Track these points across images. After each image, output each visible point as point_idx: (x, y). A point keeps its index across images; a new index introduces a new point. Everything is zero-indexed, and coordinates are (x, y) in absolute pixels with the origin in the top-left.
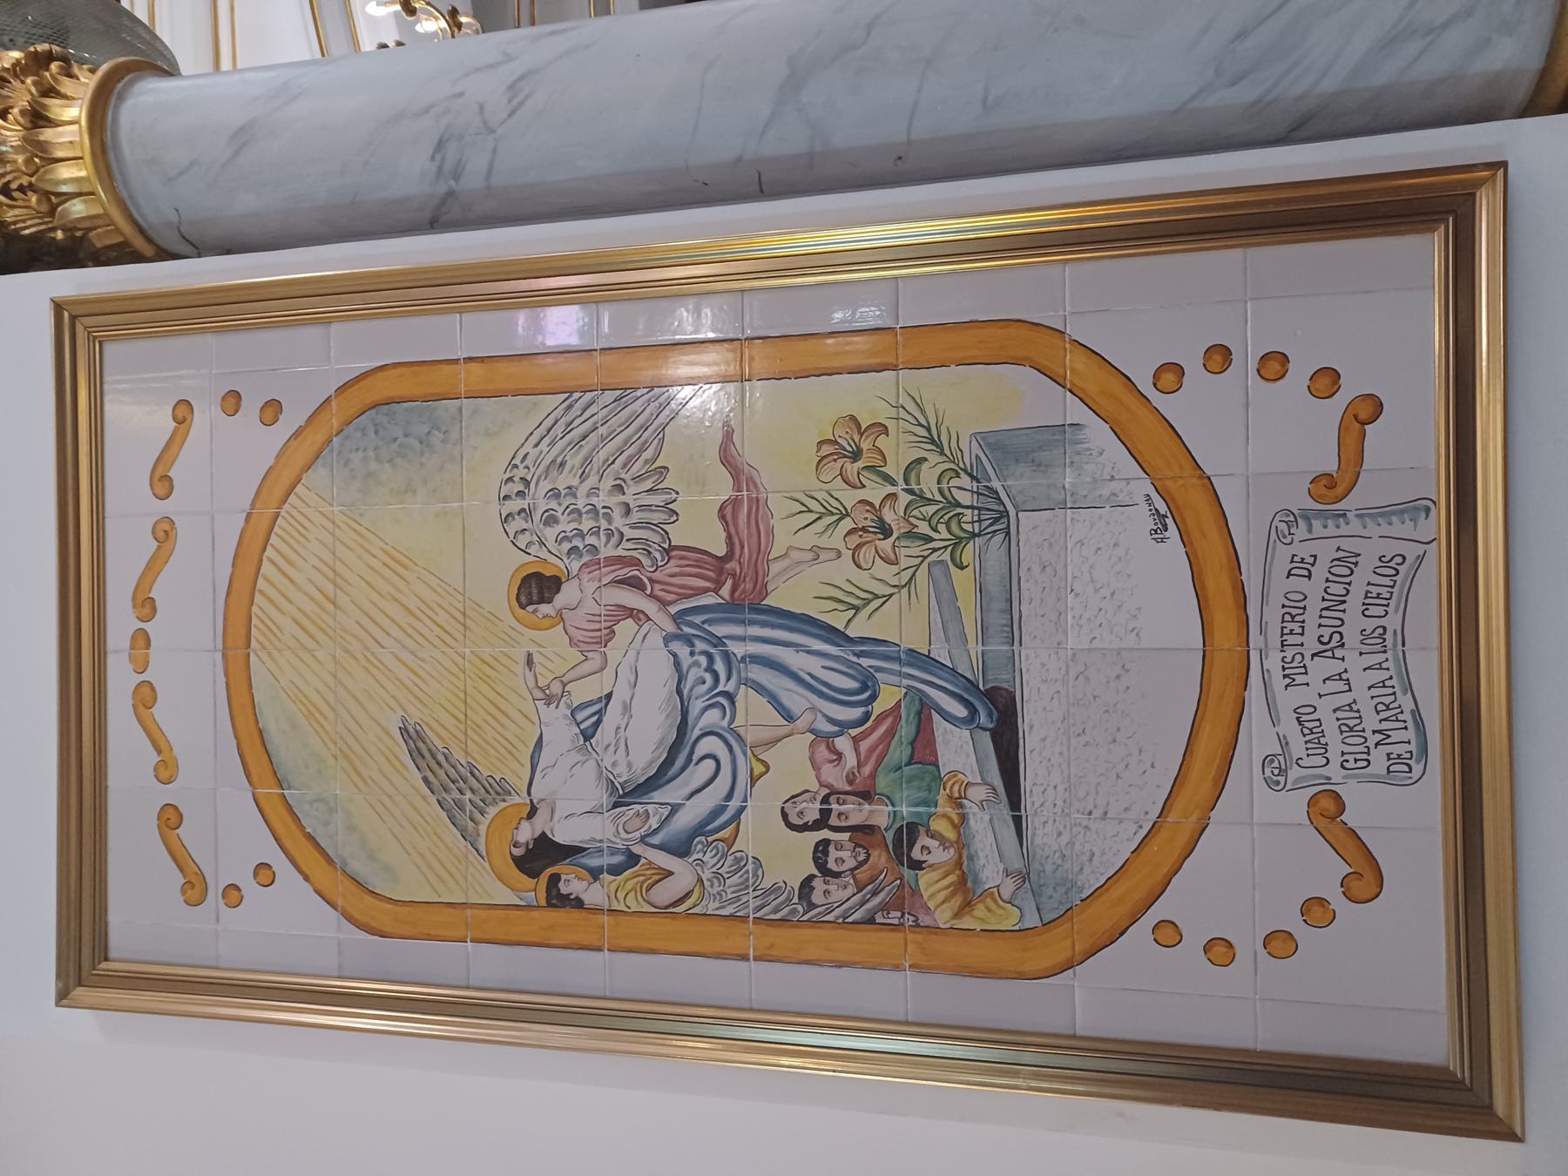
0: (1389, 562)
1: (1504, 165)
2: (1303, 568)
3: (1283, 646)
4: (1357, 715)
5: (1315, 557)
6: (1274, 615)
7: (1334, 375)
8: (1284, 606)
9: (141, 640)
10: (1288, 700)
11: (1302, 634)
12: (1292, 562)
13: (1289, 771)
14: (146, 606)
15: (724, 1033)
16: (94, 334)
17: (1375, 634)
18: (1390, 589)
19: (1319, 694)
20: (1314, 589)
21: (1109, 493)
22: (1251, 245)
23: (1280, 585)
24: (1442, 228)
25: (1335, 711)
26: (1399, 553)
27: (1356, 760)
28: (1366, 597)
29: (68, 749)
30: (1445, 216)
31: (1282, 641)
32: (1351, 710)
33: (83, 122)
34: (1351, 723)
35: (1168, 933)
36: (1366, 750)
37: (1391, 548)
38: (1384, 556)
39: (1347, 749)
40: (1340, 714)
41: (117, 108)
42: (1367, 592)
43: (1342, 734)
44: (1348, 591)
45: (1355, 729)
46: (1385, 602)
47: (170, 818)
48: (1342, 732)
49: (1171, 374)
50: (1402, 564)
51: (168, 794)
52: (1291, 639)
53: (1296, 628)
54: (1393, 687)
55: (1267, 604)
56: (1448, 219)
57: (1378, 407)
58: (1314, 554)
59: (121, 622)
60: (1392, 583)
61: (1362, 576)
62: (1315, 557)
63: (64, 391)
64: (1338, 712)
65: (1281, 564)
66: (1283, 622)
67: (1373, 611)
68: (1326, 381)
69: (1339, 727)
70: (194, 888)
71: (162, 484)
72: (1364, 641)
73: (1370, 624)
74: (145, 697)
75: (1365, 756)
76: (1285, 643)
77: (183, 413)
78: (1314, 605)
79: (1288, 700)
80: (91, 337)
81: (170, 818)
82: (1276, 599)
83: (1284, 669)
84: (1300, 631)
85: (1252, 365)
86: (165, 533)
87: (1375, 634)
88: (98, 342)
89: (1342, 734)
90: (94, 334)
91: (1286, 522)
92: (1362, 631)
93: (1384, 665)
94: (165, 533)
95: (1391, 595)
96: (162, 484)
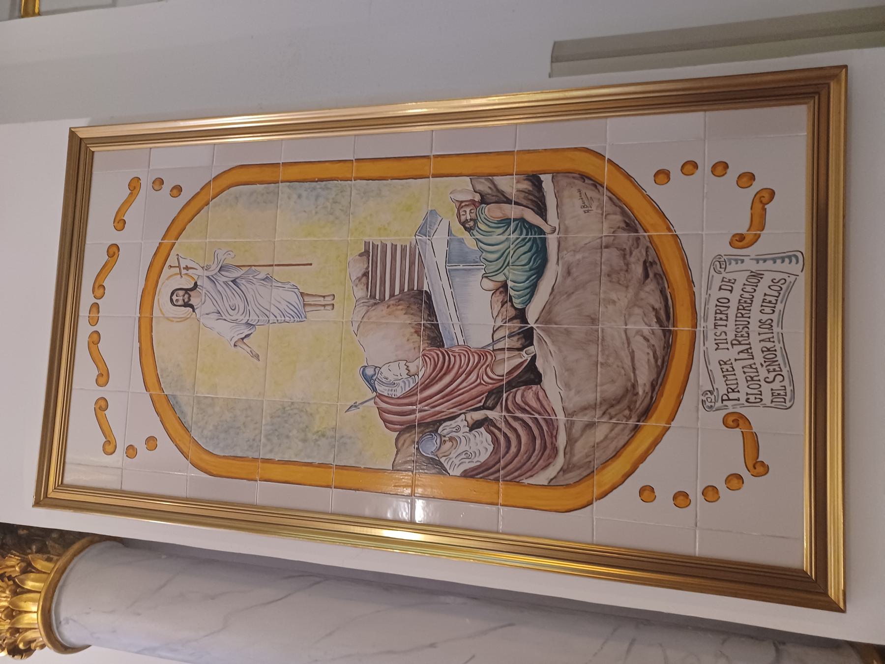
0: (777, 283)
1: (846, 67)
2: (728, 285)
3: (715, 326)
4: (755, 371)
5: (735, 280)
6: (712, 309)
7: (752, 177)
8: (717, 306)
9: (95, 307)
10: (715, 357)
11: (727, 320)
12: (723, 281)
13: (716, 403)
14: (99, 288)
15: (401, 112)
16: (56, 486)
17: (767, 323)
18: (776, 298)
19: (731, 293)
20: (734, 298)
21: (626, 299)
22: (709, 110)
23: (716, 294)
24: (812, 102)
25: (743, 368)
26: (783, 278)
27: (756, 398)
28: (763, 302)
29: (60, 300)
30: (814, 95)
31: (715, 323)
32: (751, 368)
33: (43, 594)
34: (752, 375)
35: (647, 493)
36: (760, 393)
37: (778, 276)
38: (775, 279)
39: (750, 391)
40: (746, 370)
41: (60, 633)
42: (764, 299)
43: (747, 383)
44: (755, 290)
45: (771, 349)
46: (773, 305)
47: (102, 406)
48: (747, 381)
49: (662, 176)
50: (784, 284)
51: (101, 392)
52: (720, 323)
53: (724, 317)
54: (774, 342)
55: (709, 364)
56: (815, 97)
57: (772, 194)
58: (740, 399)
59: (87, 298)
60: (777, 295)
61: (763, 287)
62: (735, 280)
63: (51, 396)
64: (745, 368)
65: (717, 282)
66: (716, 313)
67: (768, 310)
68: (747, 178)
69: (746, 378)
70: (109, 447)
71: (120, 223)
72: (761, 327)
73: (765, 317)
74: (95, 339)
75: (760, 396)
76: (716, 324)
77: (134, 185)
78: (734, 305)
79: (715, 357)
80: (59, 488)
81: (102, 406)
82: (713, 302)
83: (715, 340)
84: (726, 318)
85: (708, 169)
86: (113, 251)
87: (767, 323)
88: (61, 486)
89: (747, 383)
90: (56, 486)
91: (719, 262)
92: (766, 378)
93: (771, 340)
94: (113, 251)
95: (779, 295)
96: (120, 223)
